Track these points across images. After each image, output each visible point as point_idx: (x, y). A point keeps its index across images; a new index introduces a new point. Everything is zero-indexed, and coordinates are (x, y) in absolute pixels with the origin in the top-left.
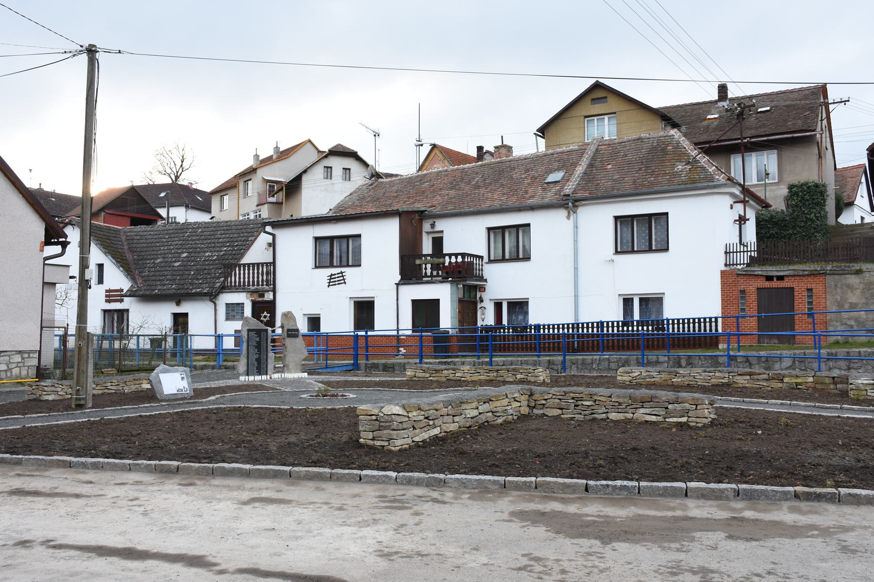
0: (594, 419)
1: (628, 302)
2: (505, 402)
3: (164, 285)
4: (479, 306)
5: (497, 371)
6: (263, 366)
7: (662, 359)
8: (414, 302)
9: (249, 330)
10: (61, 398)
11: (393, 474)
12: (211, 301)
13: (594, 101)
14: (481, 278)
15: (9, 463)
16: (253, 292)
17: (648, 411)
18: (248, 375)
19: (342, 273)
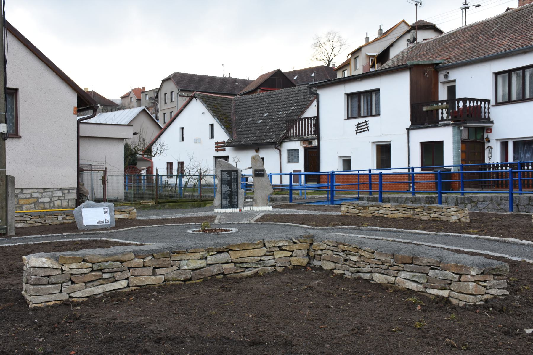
0: (360, 278)
3: (249, 137)
4: (486, 146)
5: (414, 209)
6: (234, 201)
9: (222, 171)
10: (30, 225)
12: (277, 148)
16: (305, 140)
17: (408, 275)
18: (222, 208)
19: (366, 122)
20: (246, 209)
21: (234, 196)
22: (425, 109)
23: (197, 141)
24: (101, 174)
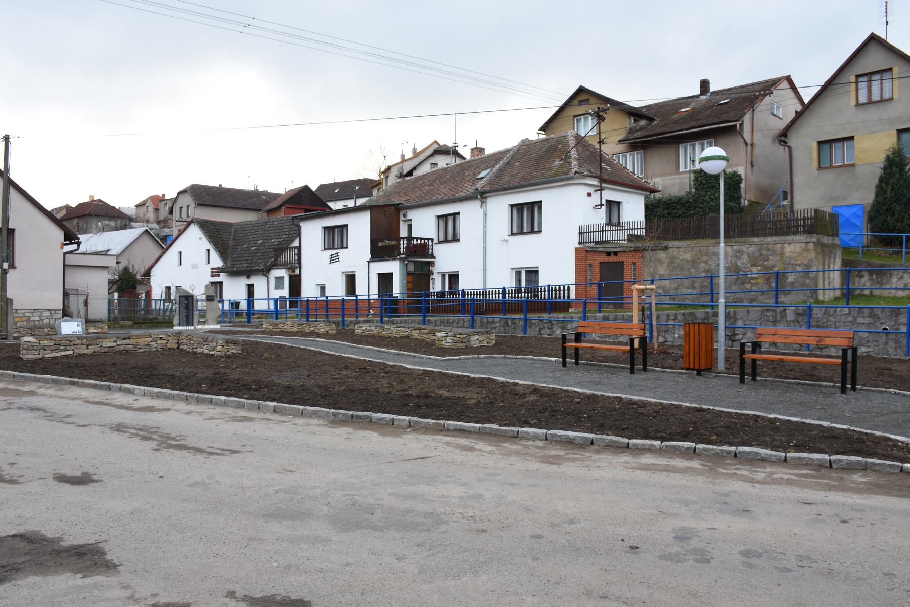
1: (518, 273)
2: (150, 340)
7: (496, 320)
8: (379, 275)
11: (657, 443)
13: (581, 103)
14: (433, 256)
15: (495, 435)
16: (289, 268)
20: (200, 327)
21: (190, 316)
22: (380, 244)
23: (194, 266)
24: (84, 298)
